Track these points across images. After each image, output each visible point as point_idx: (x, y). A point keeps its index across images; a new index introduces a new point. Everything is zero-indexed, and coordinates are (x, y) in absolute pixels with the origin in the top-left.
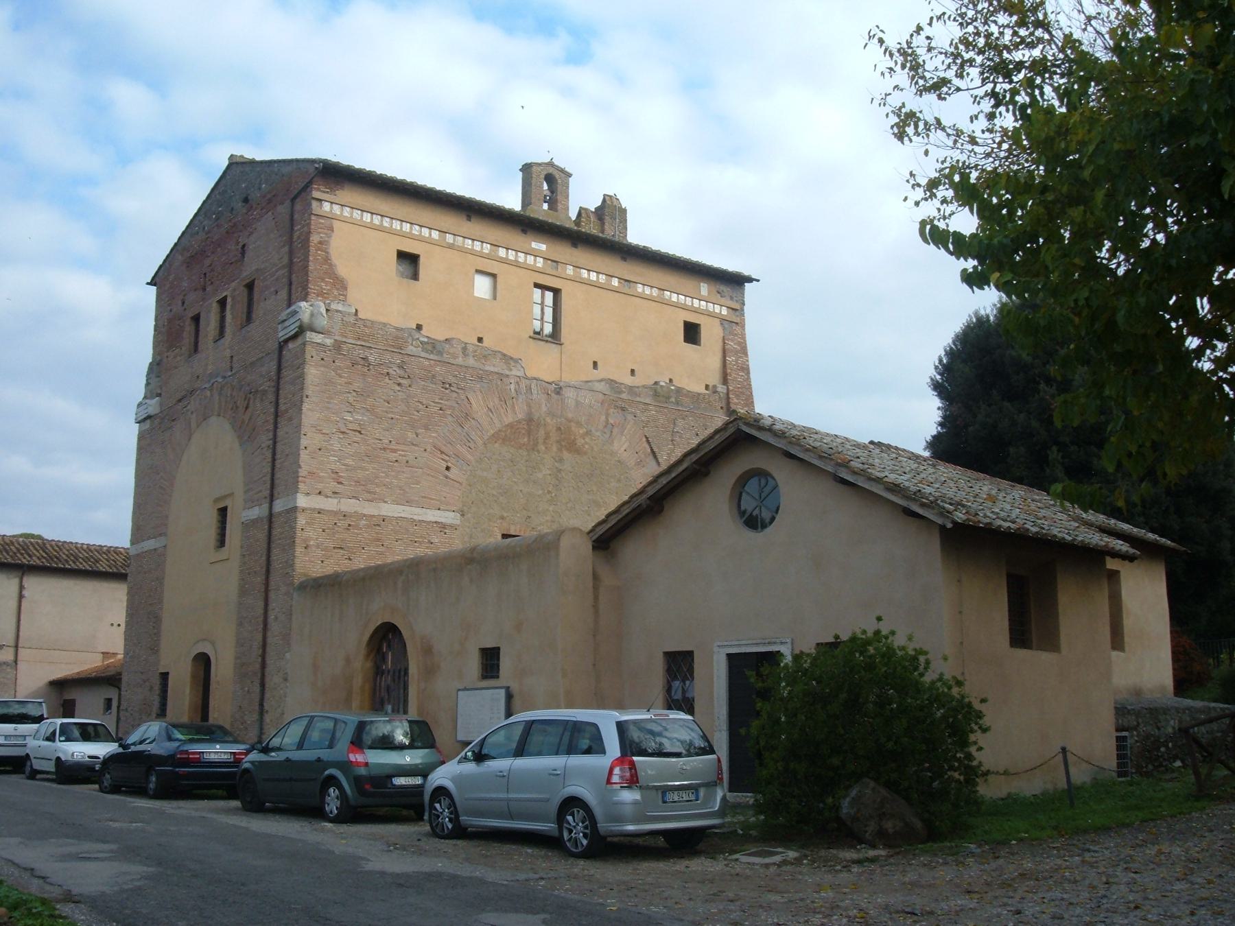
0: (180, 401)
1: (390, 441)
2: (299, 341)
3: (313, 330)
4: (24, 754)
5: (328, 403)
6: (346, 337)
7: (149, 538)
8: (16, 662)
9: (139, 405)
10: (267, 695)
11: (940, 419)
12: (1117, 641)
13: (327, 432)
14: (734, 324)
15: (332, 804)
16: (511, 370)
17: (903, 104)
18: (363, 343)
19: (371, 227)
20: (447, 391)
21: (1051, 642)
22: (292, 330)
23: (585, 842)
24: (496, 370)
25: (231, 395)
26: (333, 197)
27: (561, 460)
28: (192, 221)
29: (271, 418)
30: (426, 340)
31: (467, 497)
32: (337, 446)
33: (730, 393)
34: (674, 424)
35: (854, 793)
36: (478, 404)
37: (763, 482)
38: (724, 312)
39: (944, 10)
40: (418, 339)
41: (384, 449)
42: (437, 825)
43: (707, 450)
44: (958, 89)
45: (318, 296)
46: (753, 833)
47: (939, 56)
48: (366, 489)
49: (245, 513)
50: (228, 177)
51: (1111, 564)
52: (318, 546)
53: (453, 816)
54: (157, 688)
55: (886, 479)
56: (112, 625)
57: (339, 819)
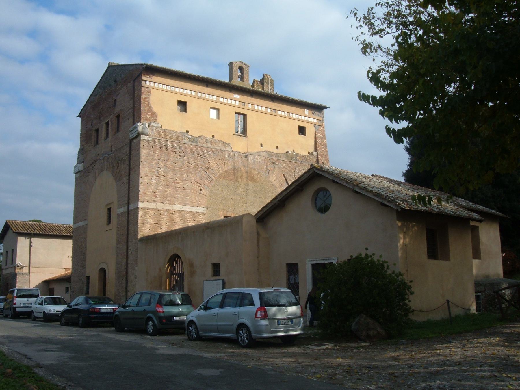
0: (91, 164)
1: (177, 179)
2: (138, 139)
3: (143, 134)
4: (31, 311)
5: (150, 164)
6: (157, 137)
7: (81, 221)
8: (29, 272)
9: (75, 167)
10: (129, 285)
11: (409, 163)
12: (477, 254)
13: (150, 176)
14: (319, 126)
15: (150, 329)
16: (226, 148)
17: (365, 40)
18: (164, 139)
19: (167, 91)
20: (200, 158)
21: (446, 257)
22: (135, 134)
23: (247, 341)
24: (220, 148)
25: (112, 162)
26: (150, 79)
27: (248, 185)
28: (94, 90)
29: (128, 171)
30: (190, 137)
31: (209, 201)
32: (154, 182)
33: (319, 155)
34: (295, 169)
35: (357, 320)
36: (213, 164)
37: (325, 193)
38: (316, 121)
39: (380, 1)
40: (187, 136)
41: (174, 182)
42: (190, 336)
43: (301, 181)
44: (388, 33)
45: (145, 120)
46: (317, 337)
47: (378, 20)
48: (167, 199)
49: (118, 210)
50: (108, 72)
51: (472, 223)
52: (148, 223)
53: (248, 337)
54: (85, 283)
55: (374, 191)
56: (68, 257)
57: (153, 334)
